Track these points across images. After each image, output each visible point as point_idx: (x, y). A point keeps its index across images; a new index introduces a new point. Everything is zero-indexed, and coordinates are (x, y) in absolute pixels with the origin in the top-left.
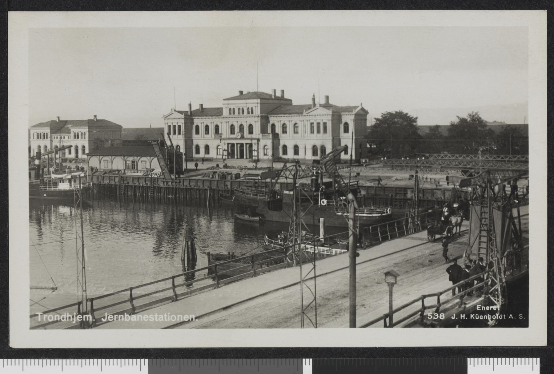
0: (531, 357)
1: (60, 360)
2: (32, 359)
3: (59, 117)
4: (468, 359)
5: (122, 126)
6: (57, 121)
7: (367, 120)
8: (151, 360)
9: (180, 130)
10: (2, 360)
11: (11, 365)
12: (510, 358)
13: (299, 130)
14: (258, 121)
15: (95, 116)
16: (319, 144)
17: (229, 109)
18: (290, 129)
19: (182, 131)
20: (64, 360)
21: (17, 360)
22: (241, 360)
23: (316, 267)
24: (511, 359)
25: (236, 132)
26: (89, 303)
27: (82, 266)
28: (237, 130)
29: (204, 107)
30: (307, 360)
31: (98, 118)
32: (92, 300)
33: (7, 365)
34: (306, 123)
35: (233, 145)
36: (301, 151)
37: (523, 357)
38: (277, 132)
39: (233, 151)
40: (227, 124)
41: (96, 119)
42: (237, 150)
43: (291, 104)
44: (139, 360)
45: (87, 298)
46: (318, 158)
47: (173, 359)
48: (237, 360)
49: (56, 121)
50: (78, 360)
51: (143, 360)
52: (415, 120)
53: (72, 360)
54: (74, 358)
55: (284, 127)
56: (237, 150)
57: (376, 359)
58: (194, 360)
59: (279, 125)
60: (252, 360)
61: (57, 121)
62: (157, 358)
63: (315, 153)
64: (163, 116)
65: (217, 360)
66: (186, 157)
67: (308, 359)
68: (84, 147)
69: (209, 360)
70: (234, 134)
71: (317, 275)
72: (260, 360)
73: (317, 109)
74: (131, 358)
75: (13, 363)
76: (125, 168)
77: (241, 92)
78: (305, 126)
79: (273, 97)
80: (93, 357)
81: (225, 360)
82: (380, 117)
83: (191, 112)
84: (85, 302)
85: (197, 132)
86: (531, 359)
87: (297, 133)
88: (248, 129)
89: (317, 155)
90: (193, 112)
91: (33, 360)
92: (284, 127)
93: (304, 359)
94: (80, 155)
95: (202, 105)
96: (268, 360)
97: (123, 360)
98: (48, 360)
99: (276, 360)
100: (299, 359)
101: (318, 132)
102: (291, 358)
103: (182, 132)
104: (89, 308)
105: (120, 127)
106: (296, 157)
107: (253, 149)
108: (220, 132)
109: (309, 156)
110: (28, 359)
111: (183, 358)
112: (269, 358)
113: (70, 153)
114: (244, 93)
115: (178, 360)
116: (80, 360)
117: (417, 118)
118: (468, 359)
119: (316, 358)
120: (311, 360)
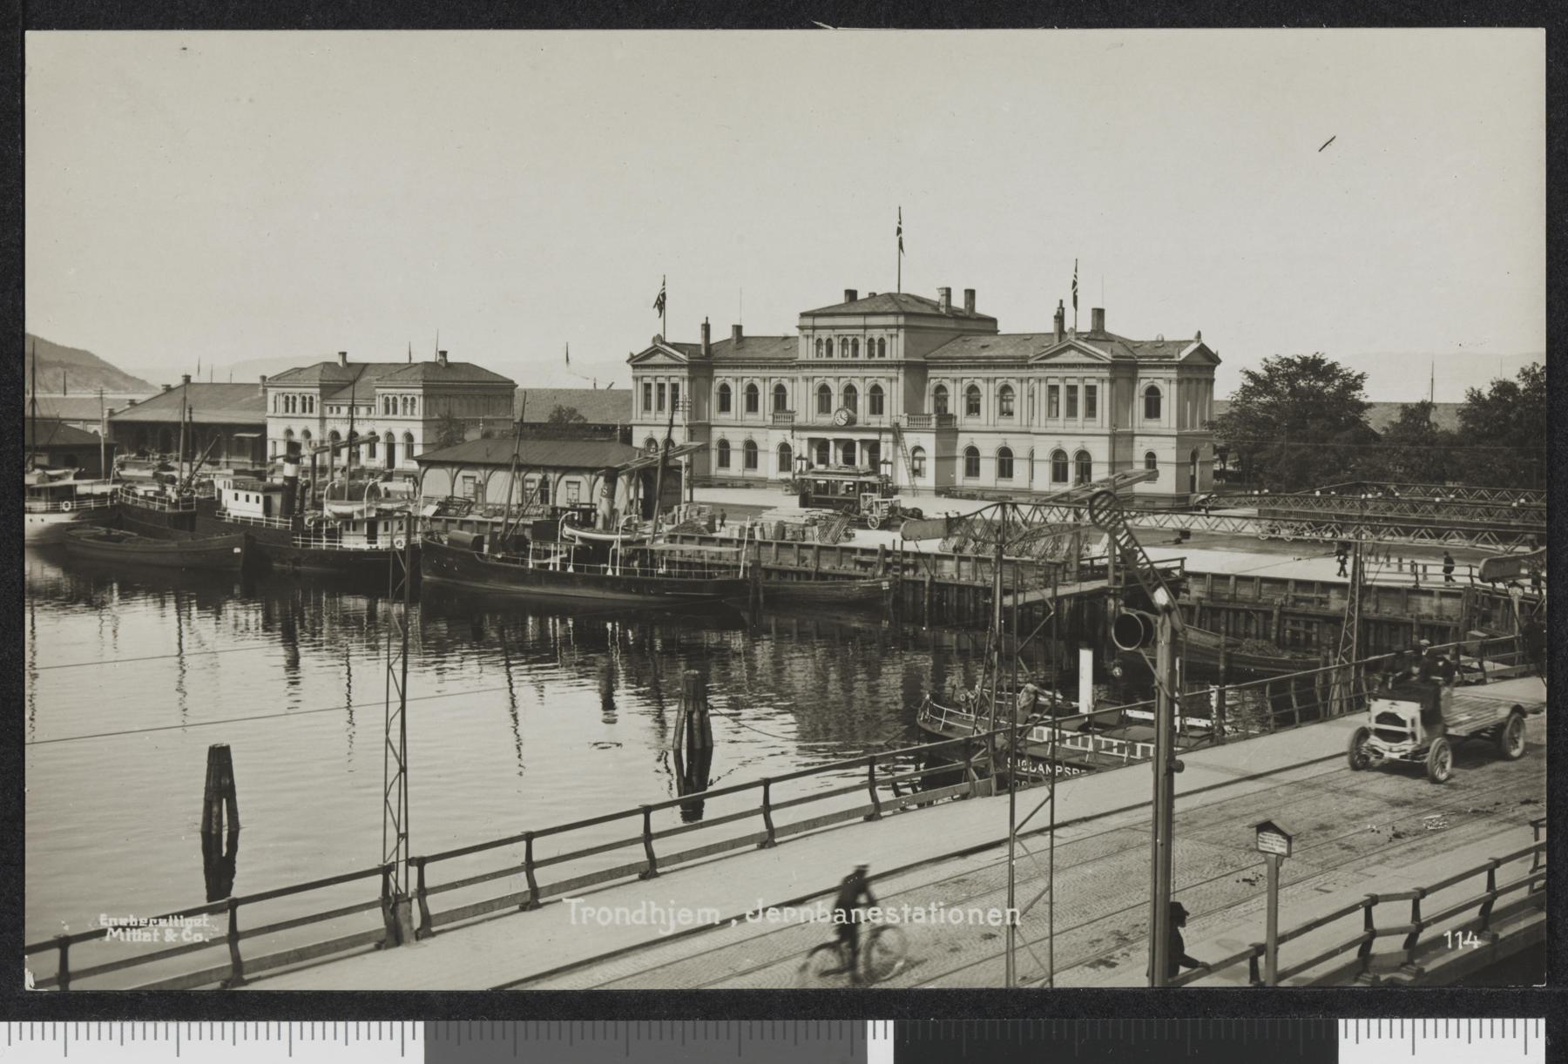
0: (1520, 1016)
1: (172, 1025)
2: (91, 1020)
3: (344, 354)
4: (1341, 1022)
5: (516, 382)
6: (341, 364)
7: (1215, 383)
8: (432, 1023)
9: (675, 396)
10: (5, 1024)
11: (32, 1038)
12: (1461, 1020)
13: (1015, 406)
14: (897, 379)
15: (444, 353)
16: (1071, 447)
17: (867, 339)
18: (989, 402)
19: (681, 399)
20: (184, 1025)
21: (49, 1025)
22: (690, 1024)
24: (1464, 1022)
25: (834, 407)
26: (414, 870)
27: (398, 766)
28: (837, 401)
29: (745, 333)
30: (880, 1024)
31: (450, 359)
32: (421, 862)
33: (21, 1038)
34: (1037, 385)
36: (1020, 469)
37: (1497, 1016)
38: (950, 410)
40: (767, 384)
41: (446, 360)
43: (995, 332)
44: (397, 1024)
45: (410, 857)
46: (1069, 486)
47: (496, 1022)
48: (678, 1024)
49: (336, 364)
50: (200, 1025)
51: (408, 1024)
52: (1356, 383)
53: (206, 1025)
54: (212, 1018)
55: (972, 394)
57: (1076, 1021)
58: (554, 1024)
60: (723, 1024)
61: (341, 364)
62: (449, 1018)
63: (1059, 474)
64: (628, 357)
65: (622, 1024)
66: (691, 473)
67: (883, 1022)
68: (409, 437)
69: (599, 1024)
70: (829, 411)
72: (745, 1024)
74: (374, 1019)
75: (37, 1034)
76: (520, 502)
77: (851, 295)
78: (1033, 396)
79: (943, 310)
80: (267, 1017)
81: (644, 1024)
82: (1260, 371)
83: (708, 346)
84: (402, 866)
85: (725, 406)
86: (1520, 1022)
87: (1011, 414)
88: (867, 400)
89: (1065, 479)
90: (713, 348)
91: (94, 1025)
92: (972, 394)
93: (870, 1023)
94: (401, 462)
95: (738, 329)
96: (767, 1023)
97: (352, 1025)
98: (139, 1025)
99: (790, 1023)
100: (857, 1023)
101: (1072, 412)
102: (832, 1019)
103: (681, 404)
104: (413, 885)
105: (511, 385)
106: (1004, 484)
107: (882, 459)
108: (789, 407)
109: (1043, 481)
110: (81, 1020)
111: (523, 1019)
112: (770, 1019)
113: (373, 454)
114: (860, 297)
115: (509, 1024)
116: (229, 1025)
117: (1361, 377)
118: (1341, 1022)
119: (906, 1017)
120: (891, 1023)
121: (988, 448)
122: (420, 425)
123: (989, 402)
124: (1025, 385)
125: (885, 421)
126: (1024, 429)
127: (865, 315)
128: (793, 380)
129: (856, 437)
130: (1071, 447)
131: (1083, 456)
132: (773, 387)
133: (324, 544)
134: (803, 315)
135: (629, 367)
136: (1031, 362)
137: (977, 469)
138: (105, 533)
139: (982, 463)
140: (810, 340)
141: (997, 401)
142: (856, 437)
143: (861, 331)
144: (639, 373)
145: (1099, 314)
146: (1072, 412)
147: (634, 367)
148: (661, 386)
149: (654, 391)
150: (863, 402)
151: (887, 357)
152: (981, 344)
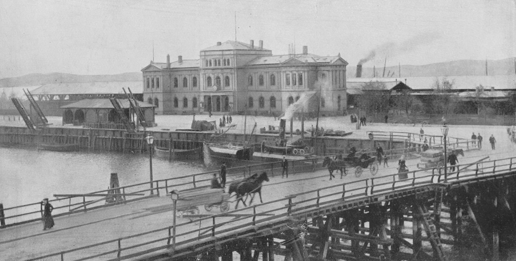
7: (347, 71)
23: (58, 201)
35: (209, 98)
39: (209, 103)
42: (213, 103)
56: (213, 103)
59: (267, 76)
71: (71, 204)
73: (148, 87)
122: (162, 94)
130: (153, 98)
134: (201, 52)
139: (265, 102)
143: (221, 57)
145: (305, 48)
151: (230, 66)
152: (265, 59)
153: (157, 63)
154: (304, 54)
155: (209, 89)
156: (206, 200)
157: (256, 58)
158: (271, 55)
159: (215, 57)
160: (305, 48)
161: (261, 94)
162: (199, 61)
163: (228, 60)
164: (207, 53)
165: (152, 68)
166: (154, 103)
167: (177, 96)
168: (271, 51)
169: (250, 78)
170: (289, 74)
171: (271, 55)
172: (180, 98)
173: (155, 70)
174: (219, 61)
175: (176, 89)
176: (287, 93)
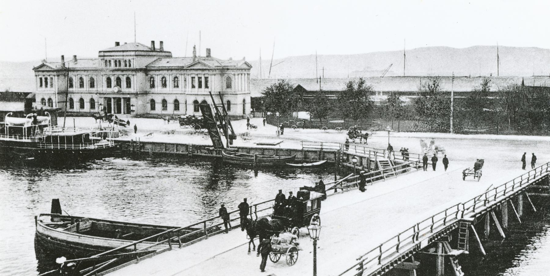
16: (200, 99)
18: (170, 83)
28: (113, 83)
35: (109, 100)
36: (182, 107)
39: (109, 105)
106: (92, 111)
121: (170, 100)
123: (170, 83)
124: (183, 76)
125: (132, 90)
126: (183, 92)
127: (123, 51)
128: (97, 75)
129: (121, 96)
131: (50, 99)
132: (116, 78)
133: (66, 147)
134: (100, 52)
135: (34, 71)
136: (184, 68)
137: (178, 107)
138: (371, 167)
139: (180, 105)
140: (103, 60)
141: (173, 82)
142: (121, 96)
144: (37, 73)
145: (209, 51)
146: (200, 86)
147: (35, 71)
148: (199, 78)
149: (196, 80)
150: (124, 83)
151: (132, 67)
153: (50, 63)
154: (207, 56)
155: (109, 90)
156: (238, 189)
157: (157, 60)
158: (170, 56)
159: (115, 58)
160: (209, 51)
161: (176, 96)
162: (96, 61)
163: (130, 61)
164: (106, 54)
165: (45, 67)
166: (47, 104)
167: (73, 96)
168: (170, 52)
169: (164, 79)
170: (194, 77)
171: (170, 56)
172: (158, 100)
173: (48, 69)
174: (120, 62)
175: (229, 90)
176: (89, 94)
